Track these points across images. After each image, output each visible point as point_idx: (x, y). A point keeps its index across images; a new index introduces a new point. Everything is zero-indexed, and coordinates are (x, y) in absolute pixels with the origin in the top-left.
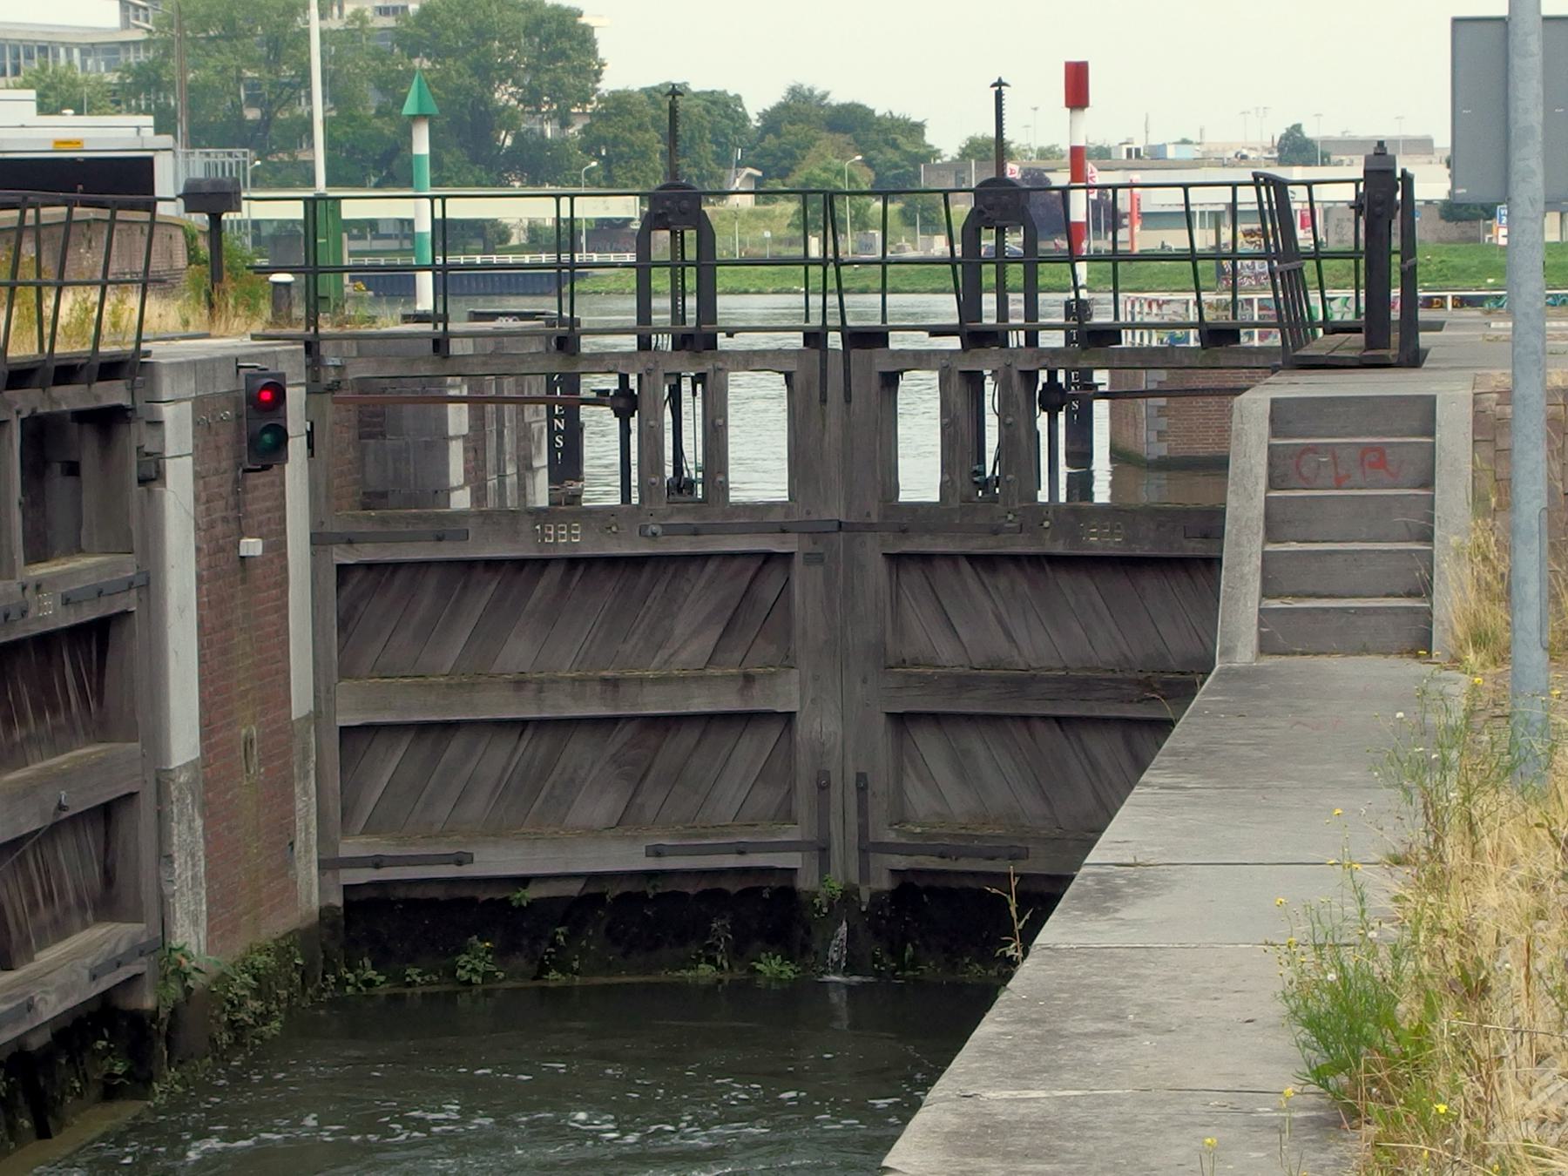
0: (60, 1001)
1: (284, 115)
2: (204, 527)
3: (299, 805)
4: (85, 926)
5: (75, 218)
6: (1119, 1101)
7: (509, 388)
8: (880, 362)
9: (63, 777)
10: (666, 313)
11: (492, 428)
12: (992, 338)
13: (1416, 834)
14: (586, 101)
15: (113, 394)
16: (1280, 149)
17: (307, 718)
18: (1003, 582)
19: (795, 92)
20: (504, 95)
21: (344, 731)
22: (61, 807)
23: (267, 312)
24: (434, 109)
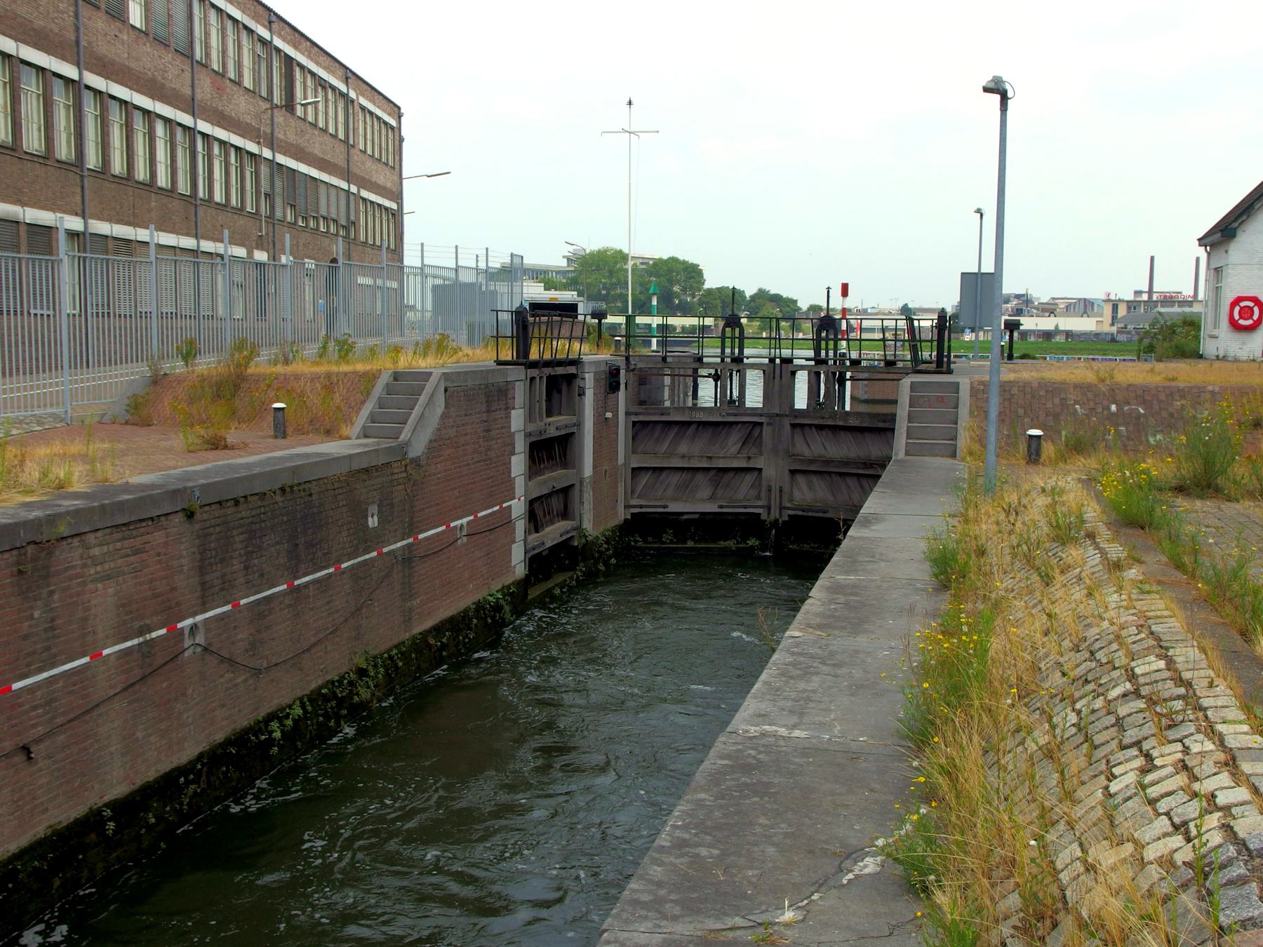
1: (613, 293)
6: (875, 580)
7: (682, 372)
8: (791, 368)
11: (677, 384)
12: (824, 362)
13: (960, 507)
18: (824, 432)
19: (760, 290)
20: (676, 289)
21: (633, 469)
23: (613, 348)
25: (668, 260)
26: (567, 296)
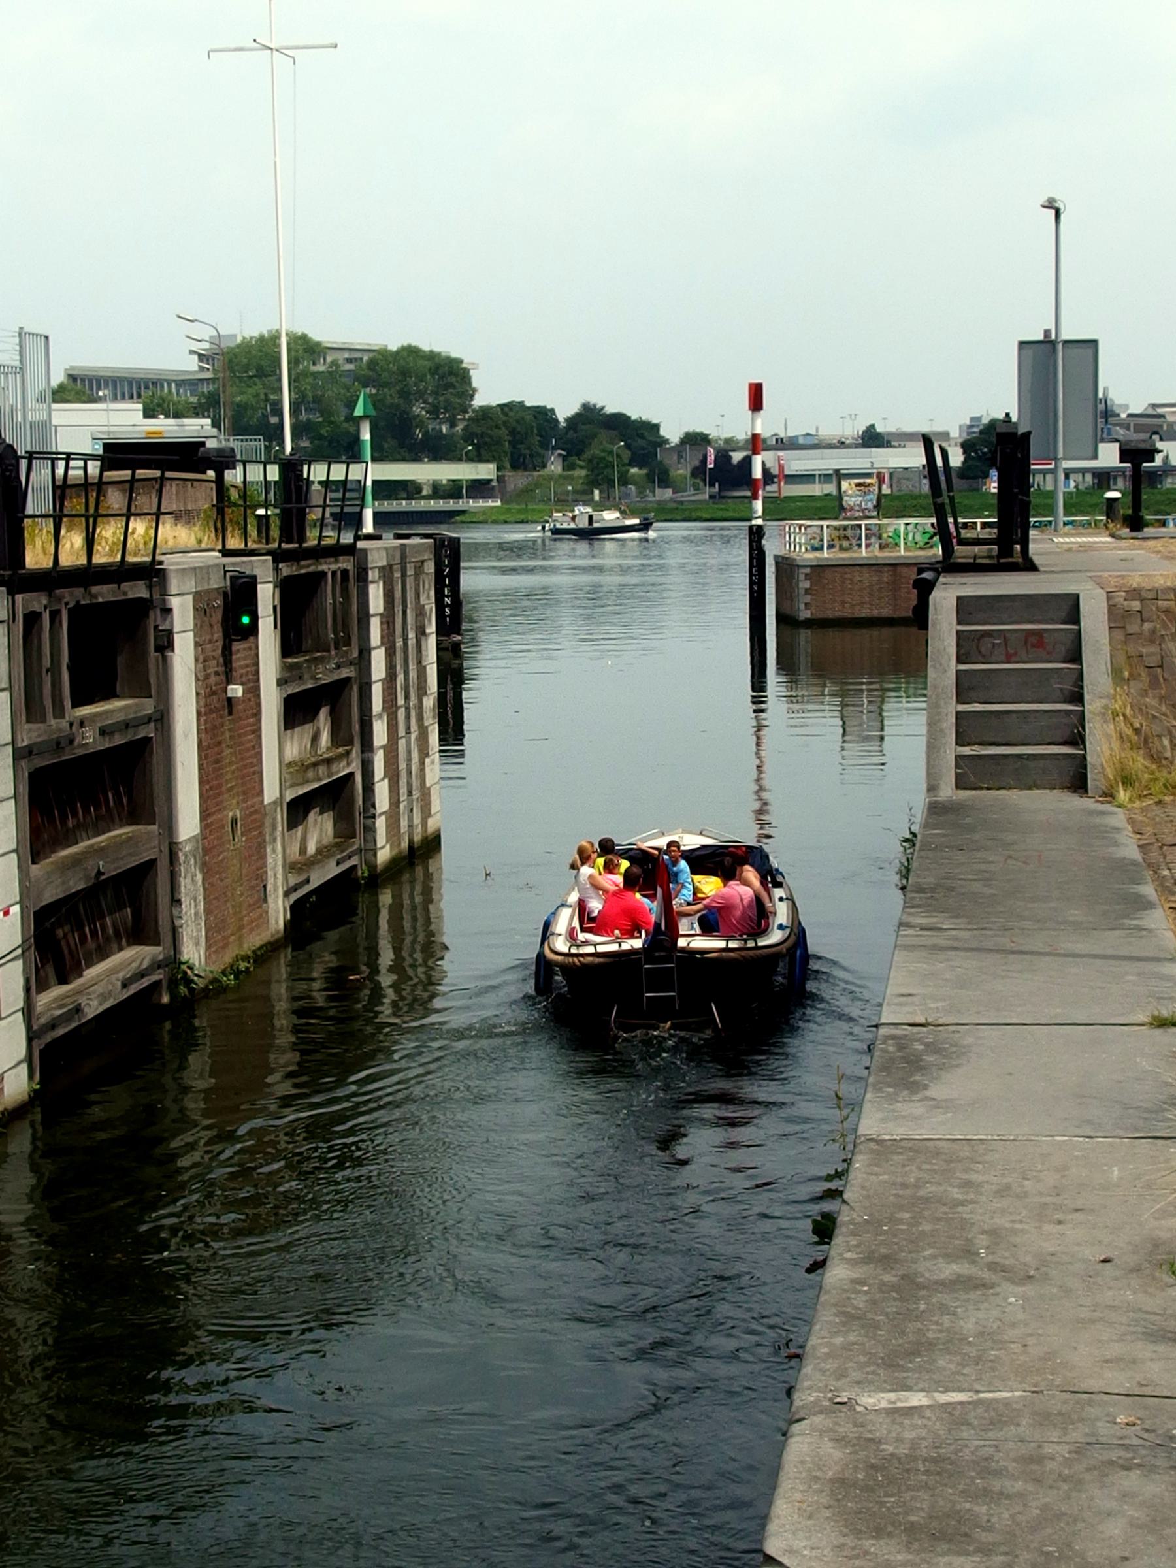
0: (101, 1004)
2: (202, 679)
3: (270, 860)
4: (121, 949)
5: (137, 477)
9: (100, 851)
10: (465, 568)
14: (465, 411)
15: (138, 590)
16: (863, 439)
17: (275, 803)
20: (418, 409)
22: (99, 873)
24: (372, 413)
25: (398, 352)
26: (196, 428)
